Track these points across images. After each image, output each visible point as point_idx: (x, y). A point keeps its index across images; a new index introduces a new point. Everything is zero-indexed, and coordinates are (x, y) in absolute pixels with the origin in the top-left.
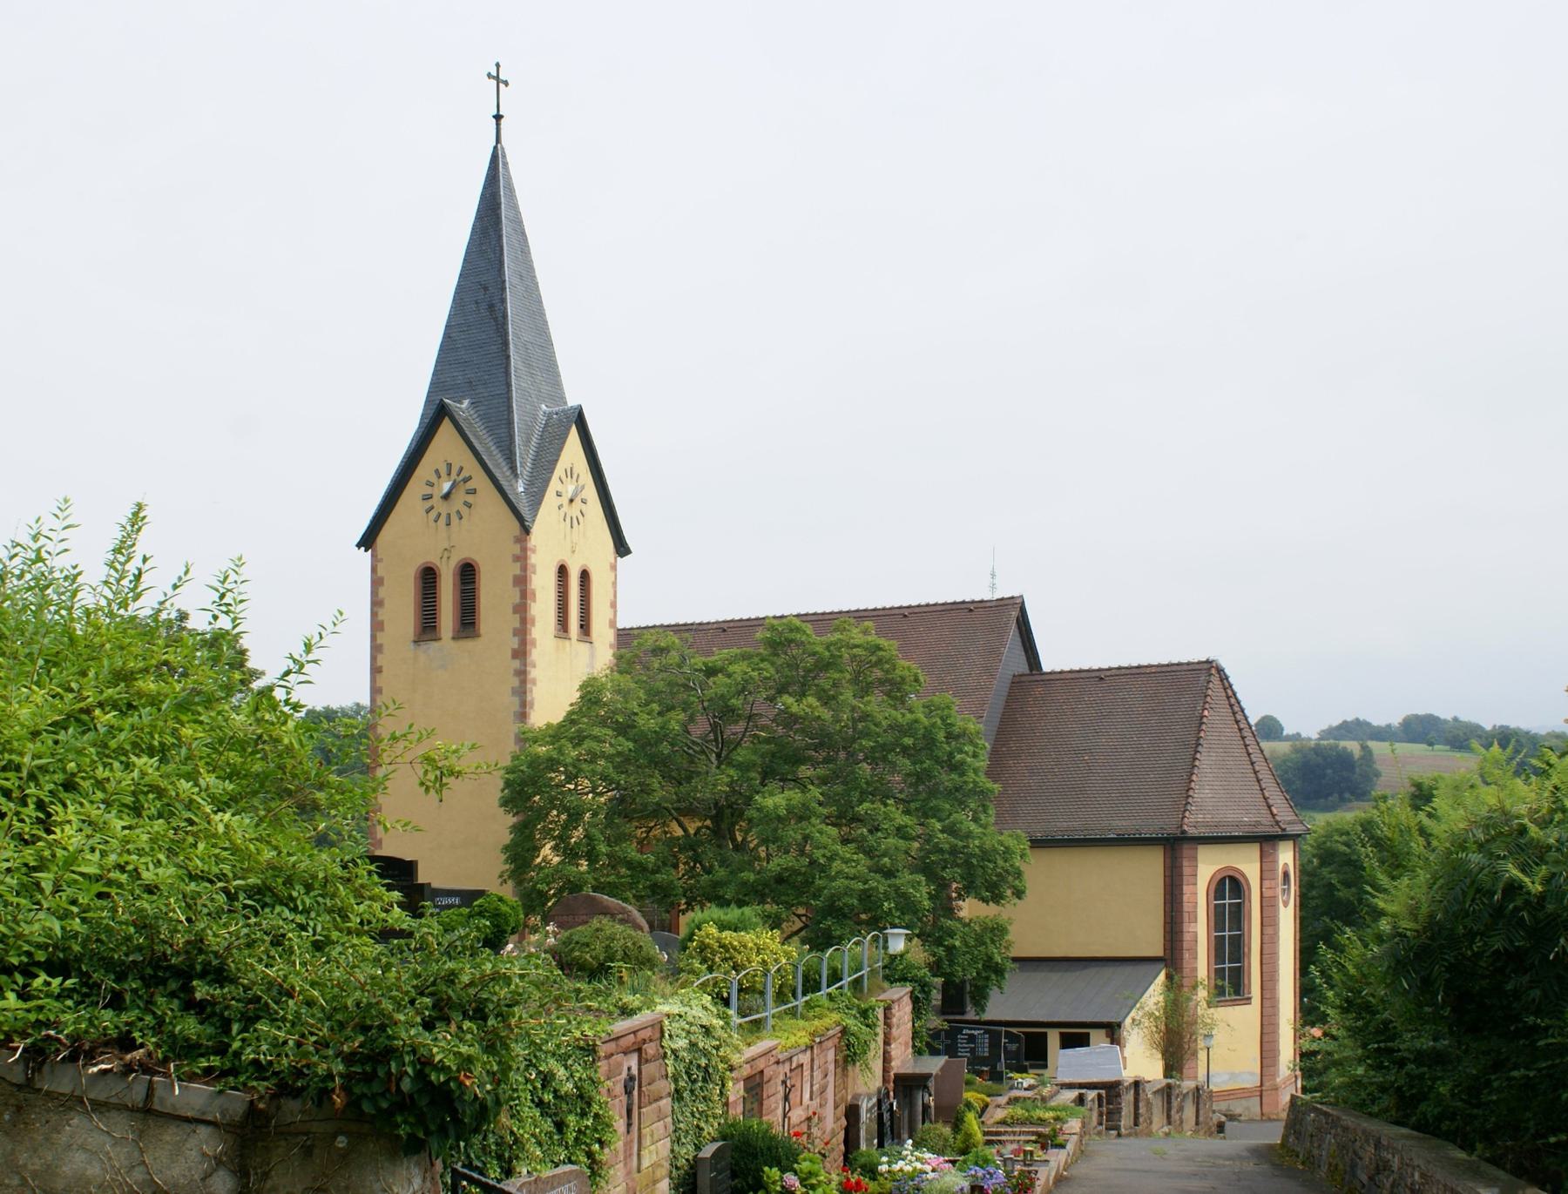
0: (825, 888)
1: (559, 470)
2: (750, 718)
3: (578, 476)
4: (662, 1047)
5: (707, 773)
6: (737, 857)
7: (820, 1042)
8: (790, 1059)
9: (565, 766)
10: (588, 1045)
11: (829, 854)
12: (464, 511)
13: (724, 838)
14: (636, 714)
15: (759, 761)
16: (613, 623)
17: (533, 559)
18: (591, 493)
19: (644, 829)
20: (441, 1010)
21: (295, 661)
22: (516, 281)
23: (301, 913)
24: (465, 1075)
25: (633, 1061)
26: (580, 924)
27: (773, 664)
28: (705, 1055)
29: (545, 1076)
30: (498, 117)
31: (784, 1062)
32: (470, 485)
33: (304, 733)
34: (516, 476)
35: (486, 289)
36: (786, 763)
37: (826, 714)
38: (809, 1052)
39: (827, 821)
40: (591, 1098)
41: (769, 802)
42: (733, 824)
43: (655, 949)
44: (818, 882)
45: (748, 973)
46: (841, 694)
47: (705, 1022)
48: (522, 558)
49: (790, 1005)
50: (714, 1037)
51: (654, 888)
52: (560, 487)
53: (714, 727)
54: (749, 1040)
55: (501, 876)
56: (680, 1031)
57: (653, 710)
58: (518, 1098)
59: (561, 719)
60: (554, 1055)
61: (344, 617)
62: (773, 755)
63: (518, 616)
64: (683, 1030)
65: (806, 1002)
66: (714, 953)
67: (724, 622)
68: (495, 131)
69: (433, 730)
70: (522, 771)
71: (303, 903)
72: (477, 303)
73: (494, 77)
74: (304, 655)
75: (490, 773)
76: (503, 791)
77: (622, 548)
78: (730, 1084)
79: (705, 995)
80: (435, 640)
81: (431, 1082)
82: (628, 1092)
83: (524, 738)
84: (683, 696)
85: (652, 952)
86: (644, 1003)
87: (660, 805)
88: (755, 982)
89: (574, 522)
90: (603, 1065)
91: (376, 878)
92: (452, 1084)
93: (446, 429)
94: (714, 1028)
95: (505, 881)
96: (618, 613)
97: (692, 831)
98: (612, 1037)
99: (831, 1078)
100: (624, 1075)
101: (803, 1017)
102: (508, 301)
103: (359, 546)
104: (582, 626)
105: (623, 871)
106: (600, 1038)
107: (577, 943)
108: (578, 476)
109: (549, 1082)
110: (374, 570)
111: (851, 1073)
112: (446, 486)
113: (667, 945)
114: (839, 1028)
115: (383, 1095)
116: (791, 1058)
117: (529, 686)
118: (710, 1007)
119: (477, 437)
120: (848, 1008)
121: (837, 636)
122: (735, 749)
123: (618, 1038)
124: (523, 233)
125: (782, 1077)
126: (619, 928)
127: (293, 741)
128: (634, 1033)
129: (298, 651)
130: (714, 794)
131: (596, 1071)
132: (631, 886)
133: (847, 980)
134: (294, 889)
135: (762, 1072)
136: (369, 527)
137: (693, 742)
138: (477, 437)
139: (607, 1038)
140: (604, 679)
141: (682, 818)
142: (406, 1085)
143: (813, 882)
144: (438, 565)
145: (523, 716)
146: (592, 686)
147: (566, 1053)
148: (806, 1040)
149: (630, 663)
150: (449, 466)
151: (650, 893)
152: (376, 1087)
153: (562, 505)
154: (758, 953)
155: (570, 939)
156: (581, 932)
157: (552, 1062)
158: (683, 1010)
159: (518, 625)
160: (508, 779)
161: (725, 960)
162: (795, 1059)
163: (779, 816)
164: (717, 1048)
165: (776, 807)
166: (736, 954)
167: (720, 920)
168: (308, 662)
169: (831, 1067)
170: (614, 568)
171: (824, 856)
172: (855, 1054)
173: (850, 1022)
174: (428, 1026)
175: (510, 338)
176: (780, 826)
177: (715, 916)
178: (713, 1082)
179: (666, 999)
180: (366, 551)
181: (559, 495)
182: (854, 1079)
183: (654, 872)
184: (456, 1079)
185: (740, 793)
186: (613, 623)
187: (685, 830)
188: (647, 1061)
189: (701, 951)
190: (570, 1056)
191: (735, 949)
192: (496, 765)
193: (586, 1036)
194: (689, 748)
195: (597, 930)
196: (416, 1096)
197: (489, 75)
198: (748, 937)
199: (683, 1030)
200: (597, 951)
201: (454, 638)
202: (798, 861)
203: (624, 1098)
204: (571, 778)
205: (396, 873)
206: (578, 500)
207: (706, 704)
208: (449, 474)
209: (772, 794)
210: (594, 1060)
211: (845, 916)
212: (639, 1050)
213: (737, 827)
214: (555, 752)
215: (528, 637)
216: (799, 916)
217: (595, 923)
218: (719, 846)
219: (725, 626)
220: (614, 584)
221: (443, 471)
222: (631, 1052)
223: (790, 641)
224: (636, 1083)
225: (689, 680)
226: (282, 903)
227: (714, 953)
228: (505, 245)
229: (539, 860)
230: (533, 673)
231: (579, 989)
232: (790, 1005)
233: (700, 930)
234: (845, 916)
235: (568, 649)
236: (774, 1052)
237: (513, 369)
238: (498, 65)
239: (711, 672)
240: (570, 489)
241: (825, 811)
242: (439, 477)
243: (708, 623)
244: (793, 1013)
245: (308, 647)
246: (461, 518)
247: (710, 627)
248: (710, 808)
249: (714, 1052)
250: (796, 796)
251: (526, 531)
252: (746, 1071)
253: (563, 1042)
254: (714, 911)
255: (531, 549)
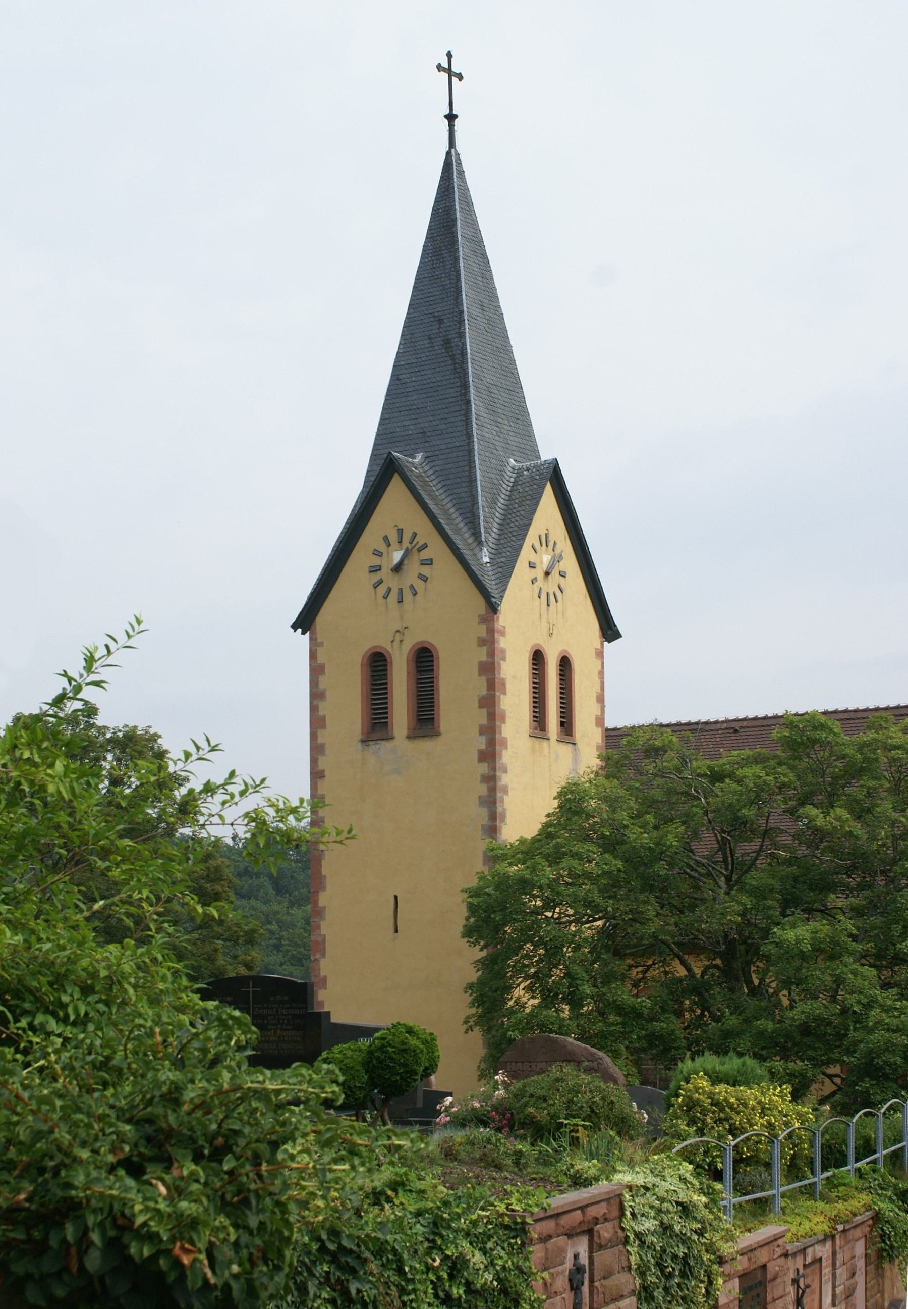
0: (861, 1042)
1: (531, 538)
2: (766, 833)
3: (555, 543)
4: (623, 1229)
5: (714, 899)
6: (753, 1004)
7: (844, 1231)
8: (803, 1251)
9: (540, 888)
10: (516, 1223)
11: (865, 1001)
12: (419, 585)
13: (737, 980)
14: (626, 827)
15: (778, 886)
16: (600, 721)
17: (503, 643)
18: (570, 563)
19: (640, 969)
20: (161, 1146)
21: (70, 680)
22: (476, 312)
23: (74, 1024)
24: (182, 1248)
25: (582, 1247)
26: (539, 1073)
27: (793, 768)
28: (684, 1242)
29: (454, 1263)
30: (451, 117)
31: (794, 1255)
32: (425, 555)
33: (78, 779)
34: (480, 543)
35: (440, 321)
36: (811, 889)
37: (857, 828)
38: (829, 1244)
39: (863, 961)
40: (519, 1295)
41: (790, 935)
42: (749, 963)
43: (631, 1106)
44: (851, 1034)
45: (748, 1139)
46: (878, 805)
47: (683, 1197)
48: (489, 642)
49: (806, 1182)
50: (695, 1218)
51: (652, 1039)
52: (533, 558)
53: (723, 845)
54: (749, 1225)
55: (465, 1022)
56: (647, 1209)
57: (648, 823)
58: (414, 1291)
59: (537, 833)
60: (468, 1234)
61: (142, 627)
62: (796, 879)
63: (484, 711)
64: (652, 1207)
65: (828, 1178)
66: (704, 1112)
67: (735, 720)
68: (447, 134)
69: (263, 781)
70: (489, 894)
71: (76, 1010)
72: (430, 339)
73: (444, 70)
74: (85, 675)
75: (341, 842)
76: (467, 919)
77: (609, 631)
78: (720, 1281)
79: (685, 1164)
80: (387, 739)
81: (130, 1258)
82: (575, 1286)
83: (493, 857)
84: (683, 808)
85: (627, 1110)
86: (602, 1171)
87: (656, 937)
88: (758, 1150)
89: (550, 600)
90: (537, 1252)
91: (185, 982)
92: (162, 1262)
93: (396, 489)
94: (694, 1206)
95: (471, 1028)
96: (606, 709)
97: (698, 971)
98: (549, 1213)
99: (860, 1278)
100: (569, 1264)
101: (823, 1198)
102: (467, 335)
103: (295, 627)
104: (562, 724)
105: (612, 1018)
106: (532, 1214)
107: (532, 1096)
108: (555, 543)
109: (459, 1271)
110: (313, 655)
111: (888, 1273)
112: (397, 556)
113: (649, 1102)
114: (869, 1214)
115: (58, 1276)
116: (805, 1249)
117: (499, 795)
118: (690, 1179)
119: (433, 498)
120: (882, 1189)
121: (872, 735)
122: (746, 872)
123: (558, 1215)
124: (484, 256)
125: (792, 1275)
126: (586, 1078)
127: (62, 789)
128: (582, 1208)
129: (76, 669)
130: (722, 925)
131: (526, 1259)
132: (625, 1035)
133: (882, 1153)
134: (65, 992)
135: (764, 1267)
136: (306, 605)
137: (697, 862)
138: (433, 498)
139: (542, 1215)
140: (587, 785)
141: (686, 957)
142: (94, 1261)
143: (846, 1035)
144: (389, 649)
145: (492, 830)
146: (572, 792)
147: (484, 1233)
148: (825, 1227)
149: (619, 765)
150: (400, 532)
151: (645, 1045)
152: (48, 1265)
153: (536, 579)
154: (763, 1114)
155: (522, 1091)
156: (537, 1083)
157: (465, 1245)
158: (651, 1180)
159: (484, 721)
160: (469, 903)
161: (718, 1121)
162: (810, 1251)
163: (802, 951)
164: (700, 1233)
165: (798, 941)
166: (733, 1114)
167: (714, 1071)
168: (87, 684)
169: (861, 1263)
170: (600, 654)
171: (859, 1002)
172: (892, 1247)
173: (884, 1206)
174: (135, 1168)
175: (471, 379)
176: (805, 964)
177: (709, 1066)
178: (696, 1278)
179: (632, 1167)
180: (303, 633)
181: (532, 566)
182: (893, 1282)
183: (651, 1019)
184: (168, 1252)
185: (756, 926)
186: (600, 721)
187: (689, 969)
188: (601, 1247)
189: (690, 1109)
190: (490, 1237)
191: (732, 1107)
192: (350, 832)
193: (513, 1210)
194: (693, 869)
195: (557, 1080)
196: (108, 1280)
197: (439, 67)
198: (751, 1094)
199: (652, 1207)
200: (557, 1106)
201: (409, 737)
202: (826, 1007)
203: (569, 1296)
204: (549, 904)
205: (286, 998)
206: (555, 573)
207: (711, 816)
208: (400, 542)
209: (793, 926)
210: (523, 1244)
211: (886, 1077)
212: (590, 1232)
213: (753, 968)
214: (528, 872)
215: (497, 736)
216: (830, 1077)
217: (554, 1071)
218: (732, 990)
219: (736, 725)
220: (601, 674)
221: (393, 538)
222: (578, 1234)
223: (814, 741)
224: (587, 1275)
225: (690, 786)
226: (47, 1011)
227: (704, 1112)
228: (462, 268)
229: (511, 1003)
230: (505, 779)
231: (520, 1151)
232: (806, 1182)
233: (688, 1082)
234: (886, 1077)
235: (546, 751)
236: (780, 1242)
237: (474, 416)
238: (449, 55)
239: (717, 777)
240: (546, 559)
241: (859, 947)
242: (389, 545)
243: (716, 722)
244: (810, 1192)
245: (90, 661)
246: (415, 594)
247: (718, 726)
248: (718, 943)
249: (695, 1237)
250: (821, 927)
251: (493, 608)
252: (742, 1264)
253: (482, 1217)
254: (710, 1061)
255: (499, 631)
